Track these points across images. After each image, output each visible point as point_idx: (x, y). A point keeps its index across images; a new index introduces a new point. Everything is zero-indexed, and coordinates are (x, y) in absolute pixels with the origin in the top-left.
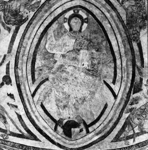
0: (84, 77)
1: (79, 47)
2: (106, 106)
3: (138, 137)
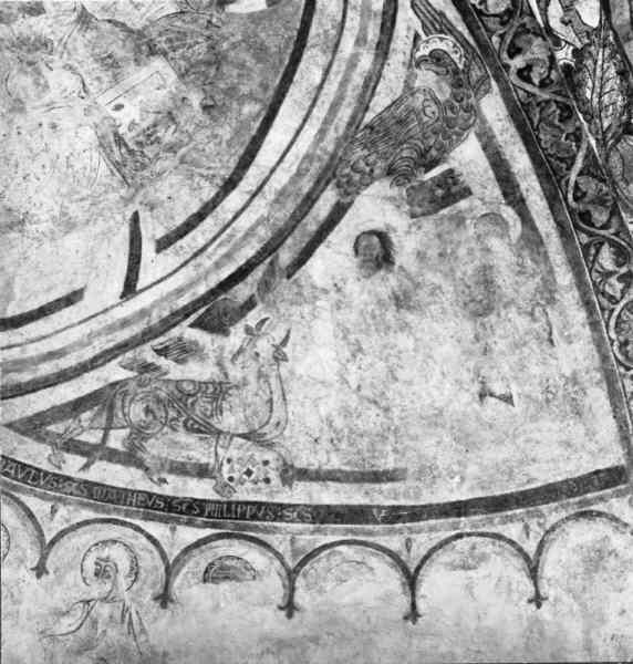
0: (84, 147)
1: (166, 42)
2: (71, 299)
3: (104, 464)
